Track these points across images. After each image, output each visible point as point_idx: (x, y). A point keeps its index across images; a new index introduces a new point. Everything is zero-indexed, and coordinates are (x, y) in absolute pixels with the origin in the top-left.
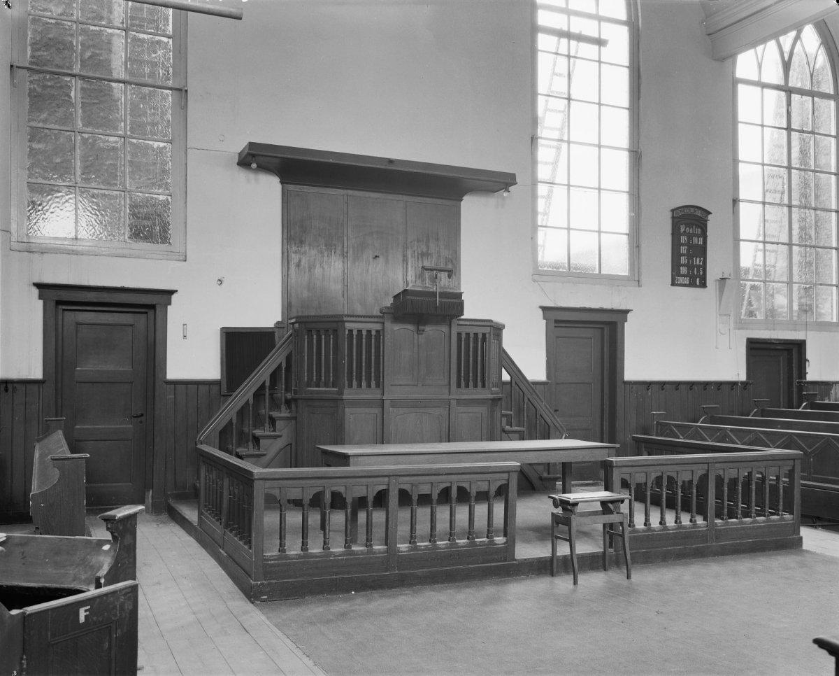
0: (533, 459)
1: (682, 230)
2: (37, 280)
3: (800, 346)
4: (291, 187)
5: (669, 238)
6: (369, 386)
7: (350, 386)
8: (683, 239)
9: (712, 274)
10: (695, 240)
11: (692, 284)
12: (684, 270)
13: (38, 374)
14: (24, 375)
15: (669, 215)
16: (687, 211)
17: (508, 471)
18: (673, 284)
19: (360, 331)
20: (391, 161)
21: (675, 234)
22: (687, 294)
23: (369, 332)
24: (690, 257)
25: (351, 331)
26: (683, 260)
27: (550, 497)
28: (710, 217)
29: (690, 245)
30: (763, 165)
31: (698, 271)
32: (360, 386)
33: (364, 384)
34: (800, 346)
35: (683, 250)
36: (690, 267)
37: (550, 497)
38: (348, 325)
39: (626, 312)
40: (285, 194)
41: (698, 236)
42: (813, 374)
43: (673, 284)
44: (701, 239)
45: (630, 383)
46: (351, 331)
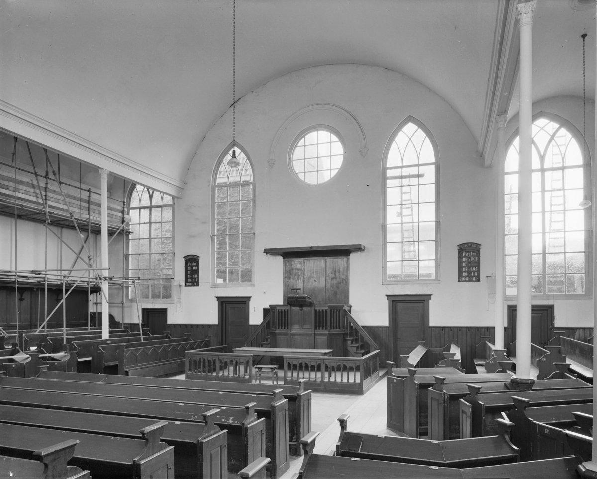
0: (256, 353)
1: (464, 255)
2: (217, 296)
3: (551, 308)
4: (286, 259)
5: (184, 268)
6: (284, 328)
7: (278, 328)
8: (189, 268)
9: (482, 276)
10: (194, 268)
11: (193, 285)
12: (189, 280)
13: (217, 323)
14: (211, 323)
15: (457, 248)
16: (194, 257)
17: (249, 356)
18: (459, 281)
19: (323, 310)
20: (311, 248)
21: (460, 256)
22: (468, 286)
23: (284, 310)
24: (191, 274)
25: (279, 310)
26: (189, 276)
27: (256, 368)
28: (481, 247)
29: (192, 270)
30: (418, 222)
31: (195, 280)
32: (281, 328)
33: (283, 328)
34: (551, 308)
35: (189, 272)
36: (192, 278)
37: (256, 368)
38: (278, 309)
39: (250, 298)
40: (285, 262)
41: (195, 266)
42: (558, 323)
43: (459, 281)
44: (196, 267)
45: (432, 327)
46: (279, 310)
